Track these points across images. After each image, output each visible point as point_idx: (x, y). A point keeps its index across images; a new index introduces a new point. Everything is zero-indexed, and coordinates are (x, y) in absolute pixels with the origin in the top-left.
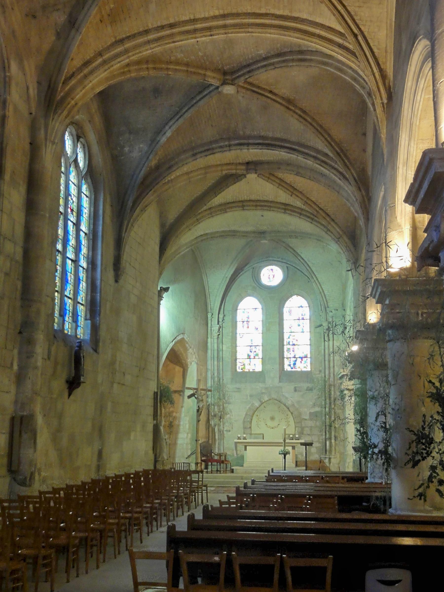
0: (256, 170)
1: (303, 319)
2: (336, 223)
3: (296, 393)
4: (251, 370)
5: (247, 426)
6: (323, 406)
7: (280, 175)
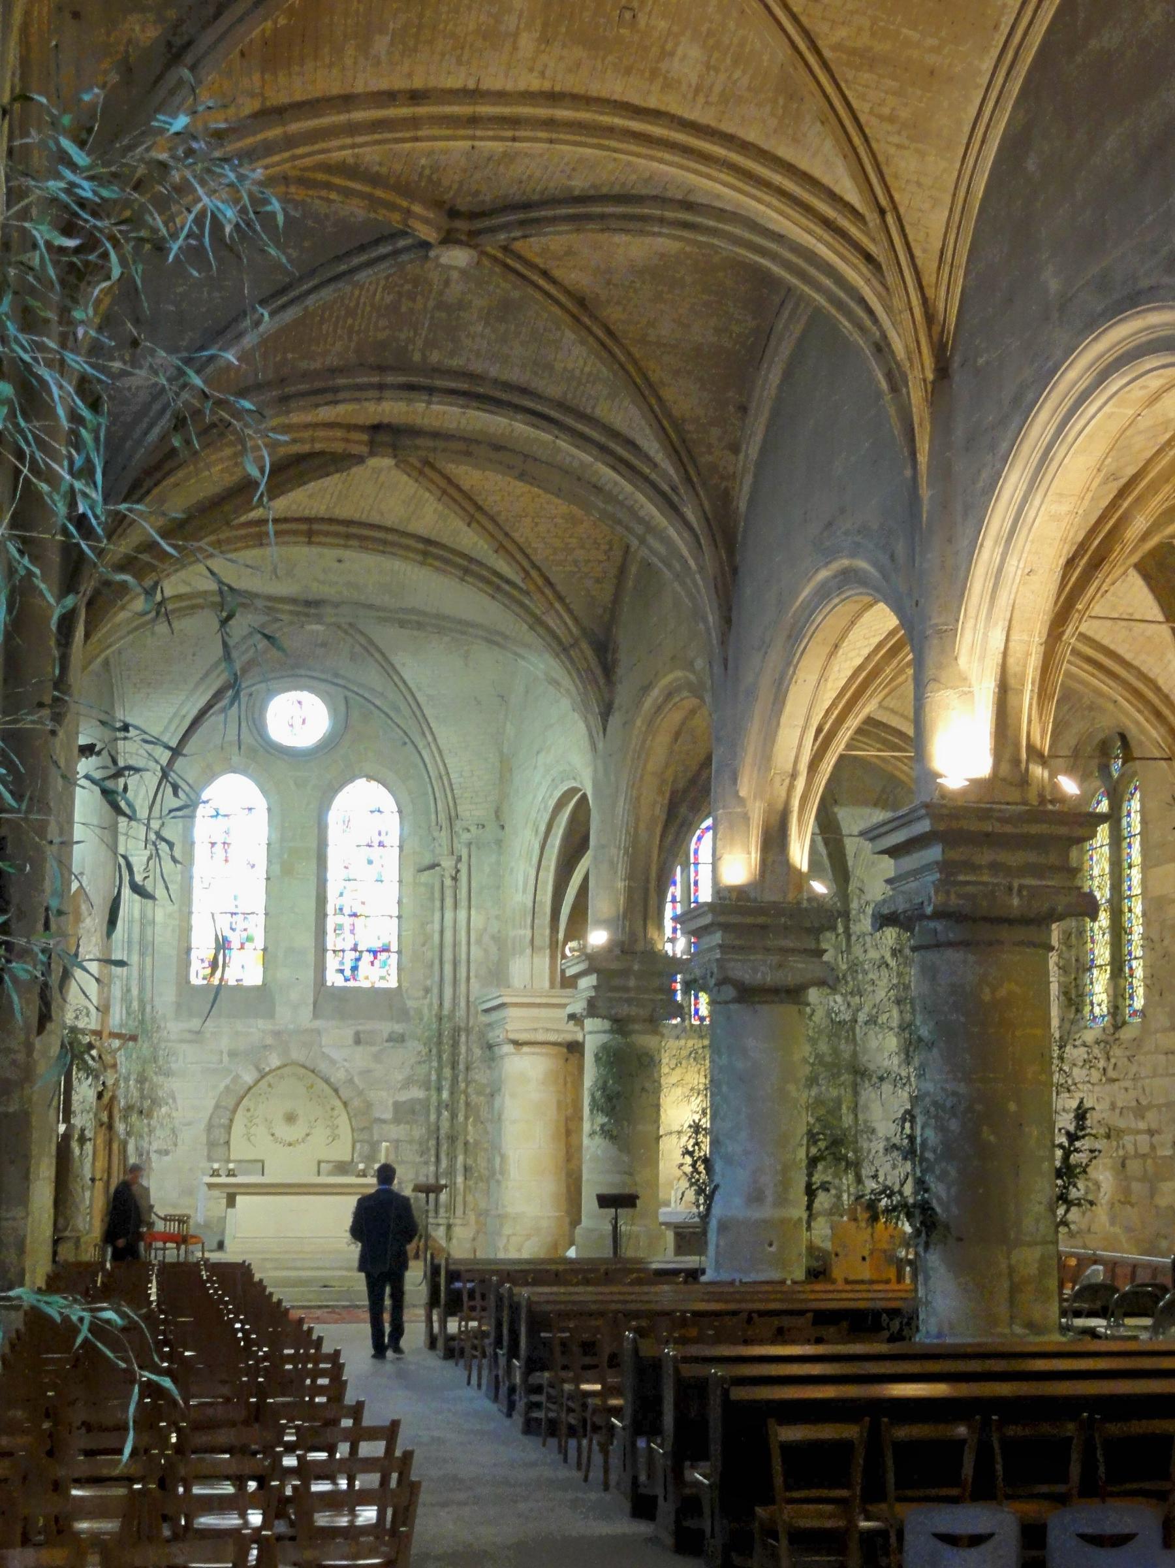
0: (395, 447)
1: (381, 844)
3: (360, 1048)
5: (218, 1139)
6: (433, 1084)
7: (451, 468)
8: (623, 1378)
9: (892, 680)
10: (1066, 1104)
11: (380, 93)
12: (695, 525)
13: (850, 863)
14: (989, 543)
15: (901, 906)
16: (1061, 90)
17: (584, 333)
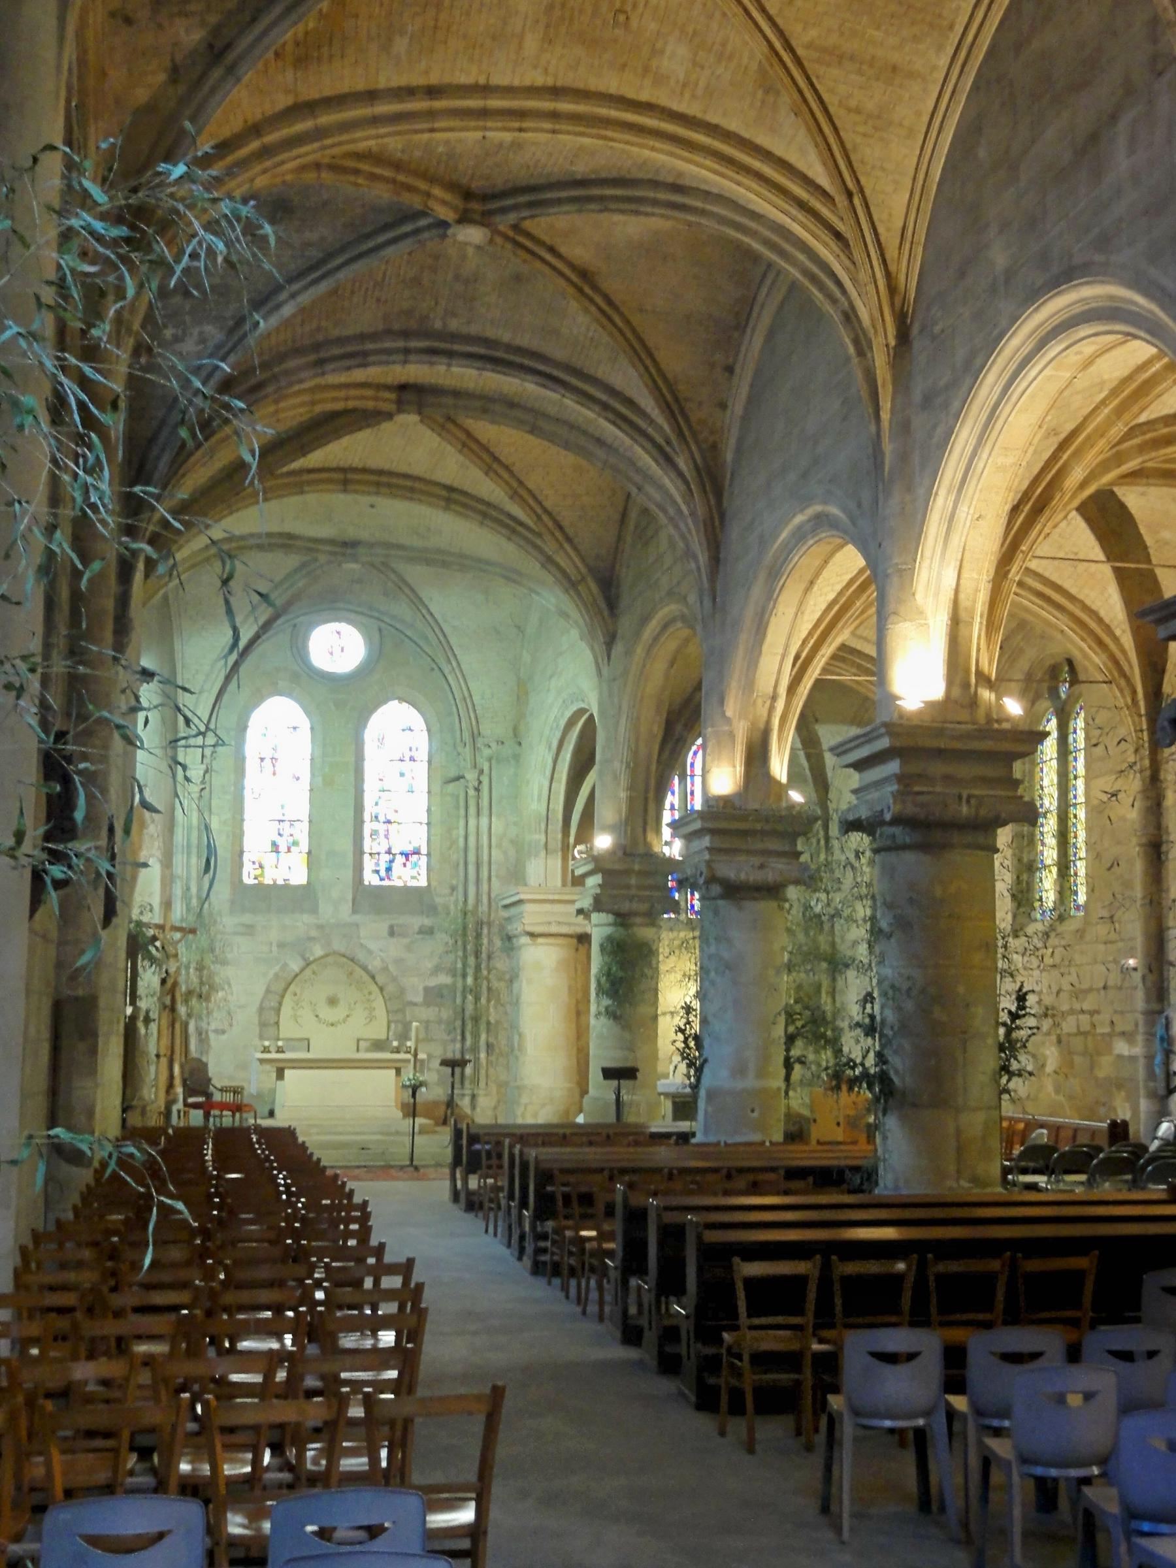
1: (412, 759)
2: (576, 549)
3: (394, 940)
4: (280, 882)
6: (459, 972)
7: (469, 423)
8: (616, 1225)
9: (862, 612)
10: (1008, 986)
11: (400, 89)
12: (687, 474)
13: (829, 774)
14: (942, 492)
15: (864, 813)
16: (1012, 86)
17: (587, 303)
